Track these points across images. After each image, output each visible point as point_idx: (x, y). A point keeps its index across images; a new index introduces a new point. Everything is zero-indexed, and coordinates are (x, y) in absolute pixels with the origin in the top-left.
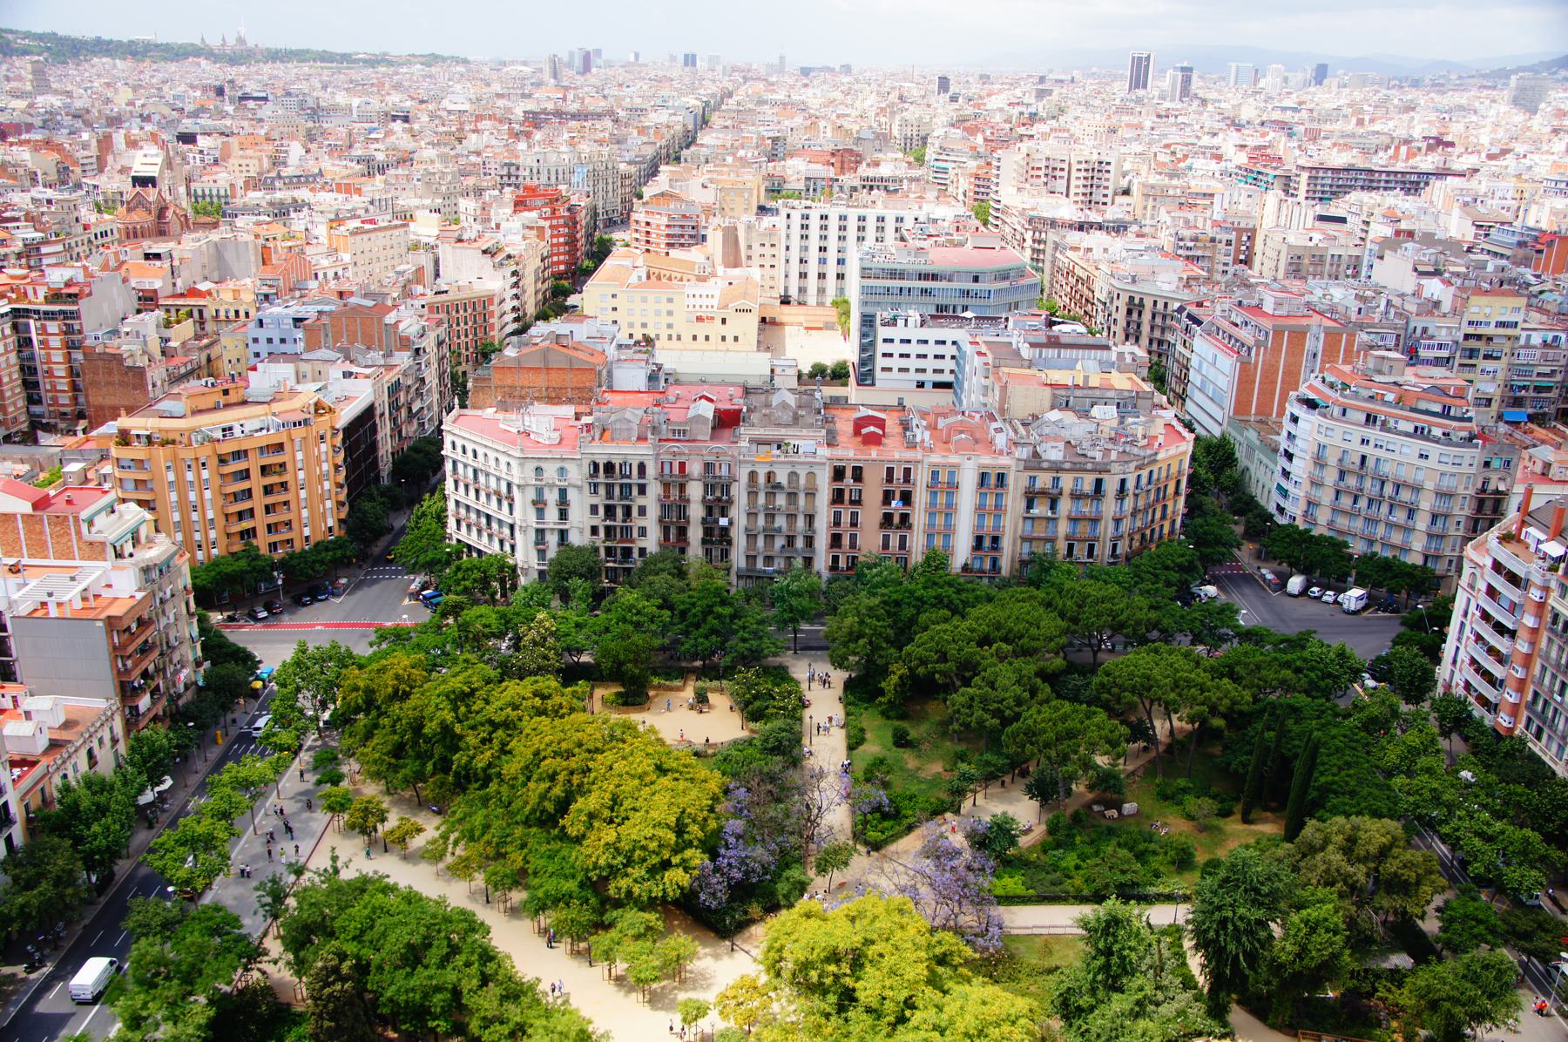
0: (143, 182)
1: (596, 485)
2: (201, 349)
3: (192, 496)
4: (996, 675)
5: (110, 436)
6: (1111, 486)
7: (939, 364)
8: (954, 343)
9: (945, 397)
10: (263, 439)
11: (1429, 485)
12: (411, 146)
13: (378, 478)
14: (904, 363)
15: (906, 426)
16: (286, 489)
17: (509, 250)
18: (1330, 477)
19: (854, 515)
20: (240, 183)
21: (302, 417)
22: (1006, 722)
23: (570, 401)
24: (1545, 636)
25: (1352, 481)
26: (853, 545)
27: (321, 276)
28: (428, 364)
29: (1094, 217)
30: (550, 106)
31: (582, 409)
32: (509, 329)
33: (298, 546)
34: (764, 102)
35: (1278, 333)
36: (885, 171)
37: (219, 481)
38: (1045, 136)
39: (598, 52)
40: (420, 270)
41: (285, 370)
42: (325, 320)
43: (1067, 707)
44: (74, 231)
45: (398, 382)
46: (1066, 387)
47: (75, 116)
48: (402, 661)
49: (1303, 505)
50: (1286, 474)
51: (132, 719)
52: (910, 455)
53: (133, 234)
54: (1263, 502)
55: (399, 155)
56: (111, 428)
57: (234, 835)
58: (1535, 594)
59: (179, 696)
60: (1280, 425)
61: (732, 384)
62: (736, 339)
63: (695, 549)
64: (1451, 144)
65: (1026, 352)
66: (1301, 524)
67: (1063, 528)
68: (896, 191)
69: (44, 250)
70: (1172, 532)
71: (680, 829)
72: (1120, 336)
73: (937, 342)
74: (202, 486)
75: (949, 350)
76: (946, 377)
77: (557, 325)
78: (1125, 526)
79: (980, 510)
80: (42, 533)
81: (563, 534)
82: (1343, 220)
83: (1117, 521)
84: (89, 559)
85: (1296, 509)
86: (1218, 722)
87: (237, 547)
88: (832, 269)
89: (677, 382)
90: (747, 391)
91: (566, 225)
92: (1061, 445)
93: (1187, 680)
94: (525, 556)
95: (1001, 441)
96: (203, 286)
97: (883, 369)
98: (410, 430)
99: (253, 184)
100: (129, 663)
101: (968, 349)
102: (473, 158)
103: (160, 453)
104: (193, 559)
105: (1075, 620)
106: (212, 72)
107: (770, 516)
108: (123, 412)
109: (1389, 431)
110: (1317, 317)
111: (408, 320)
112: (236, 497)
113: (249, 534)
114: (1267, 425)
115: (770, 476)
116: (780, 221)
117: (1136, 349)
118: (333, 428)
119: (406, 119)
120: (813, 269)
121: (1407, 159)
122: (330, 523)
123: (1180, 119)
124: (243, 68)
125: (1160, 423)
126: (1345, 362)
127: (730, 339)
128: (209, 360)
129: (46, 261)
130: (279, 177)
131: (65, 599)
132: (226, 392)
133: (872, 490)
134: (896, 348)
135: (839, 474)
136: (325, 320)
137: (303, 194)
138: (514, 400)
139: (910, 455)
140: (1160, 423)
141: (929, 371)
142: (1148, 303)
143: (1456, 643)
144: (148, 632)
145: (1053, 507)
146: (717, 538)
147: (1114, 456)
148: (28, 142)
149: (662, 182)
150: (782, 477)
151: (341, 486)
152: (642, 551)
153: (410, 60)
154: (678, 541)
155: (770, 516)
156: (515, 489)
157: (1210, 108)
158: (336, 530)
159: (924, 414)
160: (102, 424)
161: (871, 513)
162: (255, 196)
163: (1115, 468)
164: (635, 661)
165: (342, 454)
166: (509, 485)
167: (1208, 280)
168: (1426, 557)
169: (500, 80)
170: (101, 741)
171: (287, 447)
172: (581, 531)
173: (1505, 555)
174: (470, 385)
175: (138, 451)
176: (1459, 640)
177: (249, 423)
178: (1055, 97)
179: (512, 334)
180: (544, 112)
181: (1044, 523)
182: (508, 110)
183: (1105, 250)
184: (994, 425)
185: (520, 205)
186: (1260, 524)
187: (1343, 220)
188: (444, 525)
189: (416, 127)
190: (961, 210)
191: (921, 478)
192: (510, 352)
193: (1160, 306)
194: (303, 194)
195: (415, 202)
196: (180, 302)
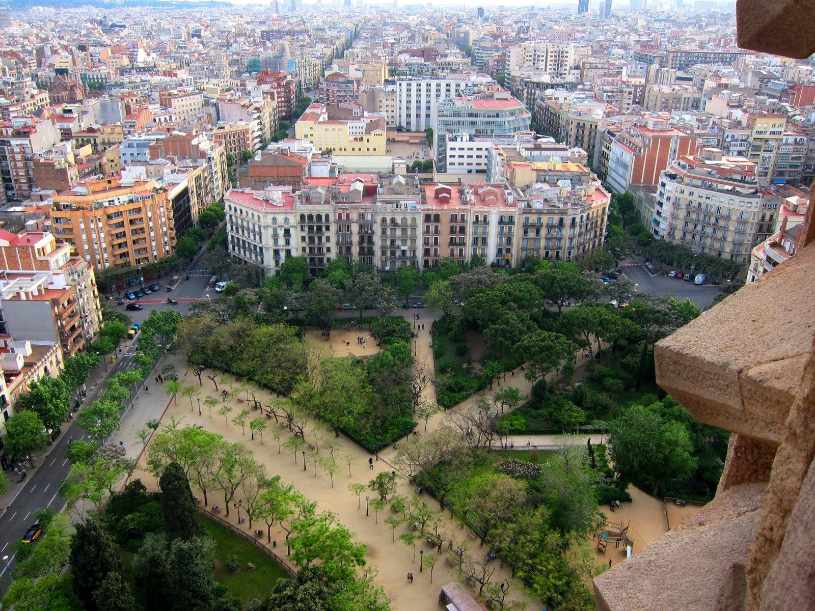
5: (50, 206)
6: (567, 221)
22: (513, 343)
59: (91, 339)
67: (543, 243)
74: (99, 231)
83: (571, 239)
86: (623, 342)
131: (29, 290)
135: (427, 218)
144: (73, 307)
145: (538, 233)
150: (399, 221)
170: (51, 363)
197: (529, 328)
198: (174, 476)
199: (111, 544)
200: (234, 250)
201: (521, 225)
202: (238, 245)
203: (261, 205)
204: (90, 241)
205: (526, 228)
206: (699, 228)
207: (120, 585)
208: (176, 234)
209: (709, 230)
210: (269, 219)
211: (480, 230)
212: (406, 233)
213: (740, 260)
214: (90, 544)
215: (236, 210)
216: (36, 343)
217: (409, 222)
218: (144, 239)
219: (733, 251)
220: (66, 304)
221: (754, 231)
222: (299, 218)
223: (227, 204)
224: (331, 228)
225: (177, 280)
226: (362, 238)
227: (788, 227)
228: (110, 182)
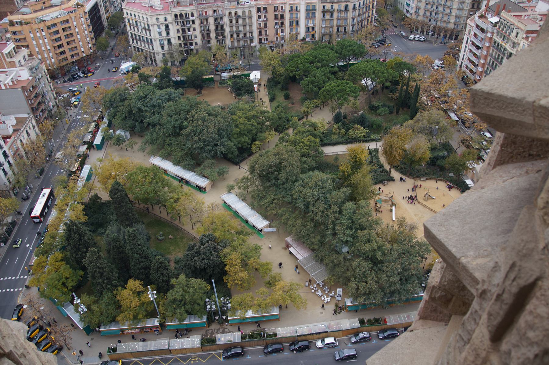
1: (177, 22)
3: (41, 42)
4: (316, 73)
5: (7, 23)
6: (351, 7)
16: (73, 36)
21: (72, 9)
22: (320, 89)
24: (492, 48)
26: (266, 34)
37: (49, 35)
43: (340, 82)
49: (415, 9)
56: (6, 20)
58: (489, 35)
59: (51, 110)
63: (214, 41)
67: (335, 22)
71: (220, 134)
74: (43, 38)
78: (356, 20)
83: (353, 19)
86: (388, 84)
93: (378, 70)
98: (112, 10)
100: (33, 101)
103: (26, 28)
108: (9, 14)
113: (63, 53)
115: (236, 13)
118: (85, 12)
122: (90, 45)
131: (6, 82)
135: (259, 10)
143: (465, 45)
144: (36, 90)
145: (332, 15)
150: (240, 13)
154: (208, 38)
155: (237, 27)
156: (150, 26)
158: (92, 48)
160: (2, 19)
165: (89, 21)
166: (148, 25)
168: (455, 25)
170: (29, 127)
171: (70, 21)
172: (175, 38)
173: (480, 22)
176: (465, 52)
181: (329, 21)
197: (328, 79)
198: (117, 189)
199: (87, 232)
200: (133, 42)
201: (321, 11)
202: (136, 38)
203: (148, 11)
204: (38, 45)
205: (324, 14)
206: (435, 7)
207: (97, 255)
208: (94, 35)
209: (441, 9)
210: (154, 21)
211: (294, 16)
212: (246, 22)
213: (459, 28)
214: (75, 233)
215: (131, 15)
216: (17, 116)
217: (247, 14)
218: (74, 40)
219: (455, 22)
220: (31, 89)
221: (469, 8)
222: (174, 17)
223: (125, 12)
224: (196, 22)
225: (99, 66)
226: (217, 27)
227: (490, 5)
228: (44, 3)
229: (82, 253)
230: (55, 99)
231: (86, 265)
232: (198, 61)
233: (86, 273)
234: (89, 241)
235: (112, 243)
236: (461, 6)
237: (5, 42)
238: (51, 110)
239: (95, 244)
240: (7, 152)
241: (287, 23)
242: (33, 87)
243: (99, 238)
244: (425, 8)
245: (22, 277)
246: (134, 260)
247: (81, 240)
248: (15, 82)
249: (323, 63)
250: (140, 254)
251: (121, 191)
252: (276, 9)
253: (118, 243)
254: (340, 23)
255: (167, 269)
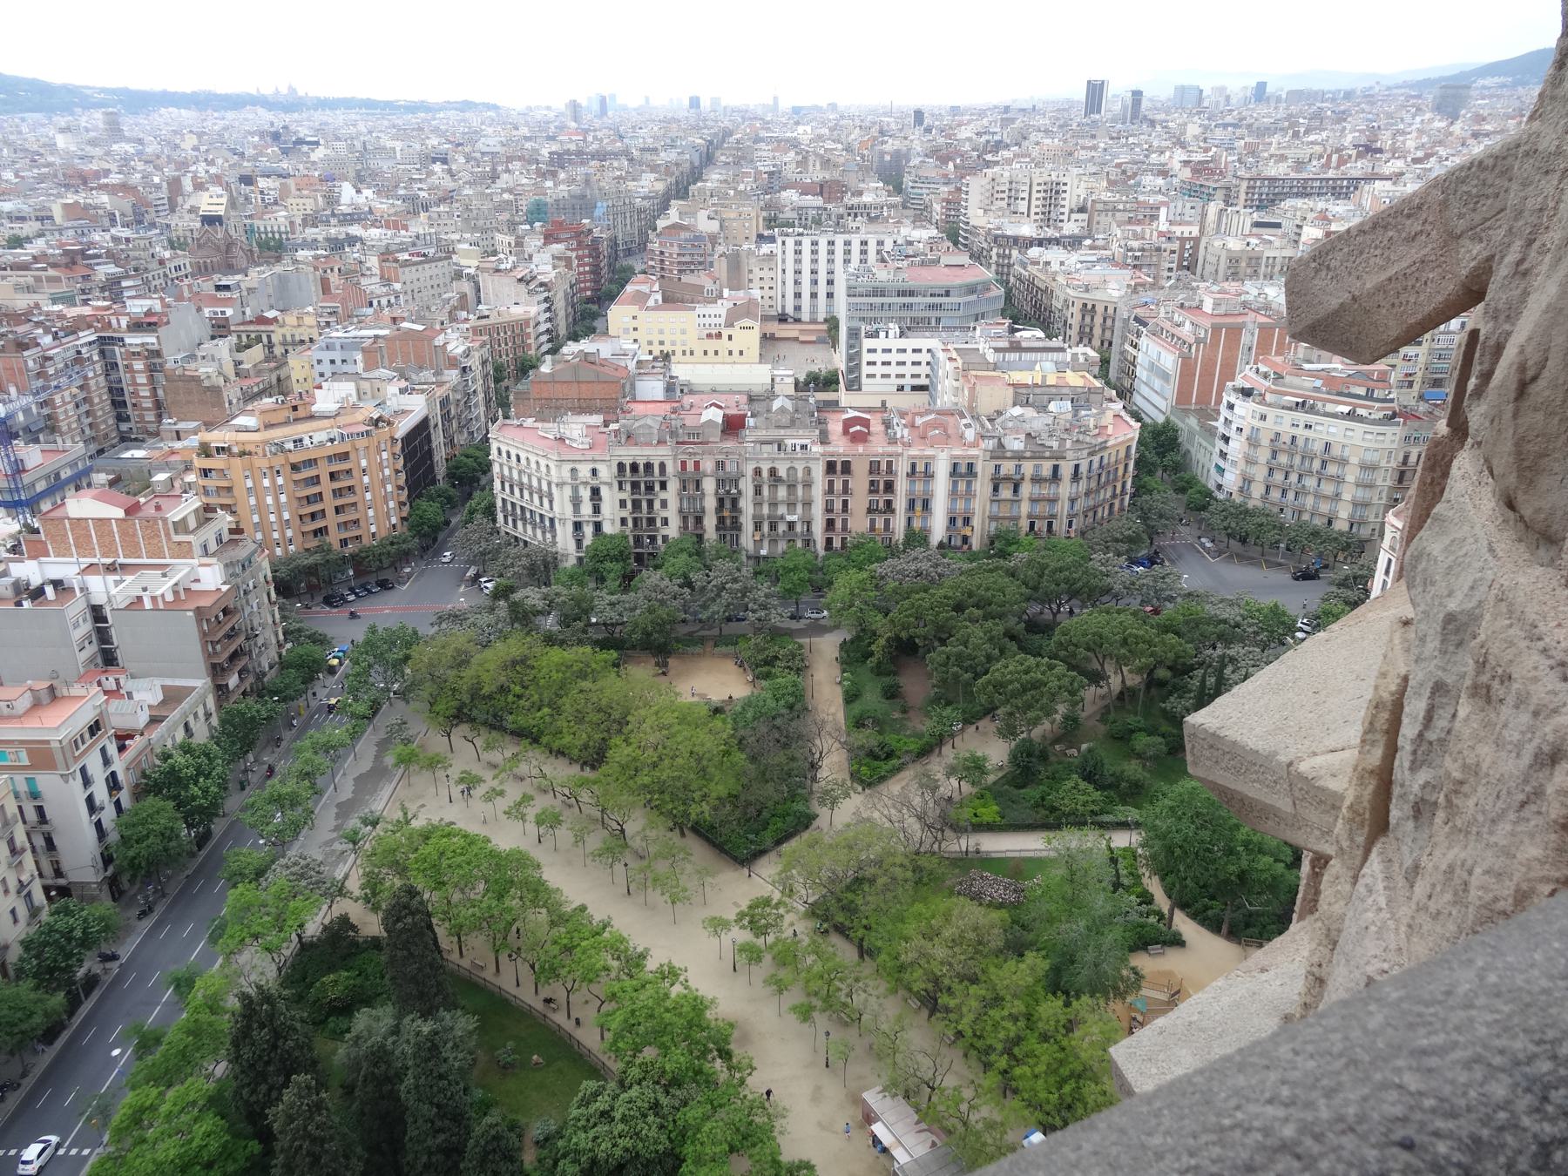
0: (210, 220)
2: (271, 370)
3: (269, 500)
6: (1066, 470)
7: (916, 370)
8: (929, 351)
9: (921, 398)
10: (331, 449)
11: (1354, 460)
12: (451, 185)
13: (434, 481)
14: (886, 370)
15: (887, 425)
17: (541, 278)
18: (1263, 455)
19: (846, 483)
20: (298, 221)
22: (977, 676)
23: (598, 411)
25: (1283, 459)
26: (845, 528)
27: (375, 303)
28: (474, 380)
29: (1050, 233)
30: (573, 147)
31: (611, 417)
32: (545, 348)
33: (366, 541)
34: (761, 140)
35: (1216, 329)
36: (867, 198)
38: (1009, 162)
39: (613, 97)
40: (463, 297)
41: (347, 388)
42: (381, 343)
43: (1031, 661)
44: (150, 267)
45: (448, 397)
46: (1026, 386)
47: (147, 162)
48: (460, 637)
50: (1223, 455)
51: (221, 690)
52: (891, 449)
53: (202, 270)
54: (1203, 481)
55: (440, 193)
57: (319, 793)
59: (264, 674)
60: (1218, 413)
61: (740, 393)
62: (741, 353)
64: (1380, 151)
65: (991, 357)
66: (1237, 498)
67: (1025, 508)
68: (877, 217)
69: (124, 284)
70: (1122, 509)
72: (1075, 338)
73: (914, 351)
75: (924, 357)
76: (923, 381)
77: (586, 345)
79: (953, 494)
80: (135, 535)
81: (598, 526)
82: (1278, 226)
83: (1073, 501)
84: (178, 557)
85: (1231, 480)
86: (1162, 673)
87: (313, 543)
88: (822, 289)
89: (691, 392)
90: (751, 399)
91: (590, 256)
92: (1023, 437)
93: (1136, 637)
94: (565, 541)
95: (970, 435)
96: (270, 314)
97: (868, 376)
98: (462, 439)
99: (312, 220)
100: (218, 647)
101: (941, 356)
102: (506, 196)
104: (271, 556)
105: (1035, 589)
106: (266, 118)
107: (774, 505)
109: (1317, 413)
110: (1252, 315)
111: (456, 344)
112: (309, 500)
114: (1207, 413)
115: (773, 472)
116: (776, 248)
117: (1089, 351)
118: (392, 438)
119: (444, 161)
120: (806, 290)
121: (1338, 167)
122: (394, 520)
123: (1131, 140)
124: (296, 115)
125: (1110, 414)
126: (1278, 353)
127: (736, 353)
128: (279, 380)
129: (126, 294)
130: (333, 215)
131: (159, 593)
132: (295, 408)
133: (860, 481)
134: (879, 357)
135: (831, 467)
136: (381, 343)
137: (355, 230)
138: (551, 409)
139: (891, 449)
140: (1110, 414)
141: (908, 376)
142: (1100, 309)
145: (1016, 491)
146: (729, 525)
147: (1068, 444)
148: (107, 185)
149: (673, 215)
150: (782, 473)
151: (400, 488)
152: (665, 538)
153: (447, 106)
155: (774, 505)
157: (1158, 128)
158: (399, 527)
159: (902, 414)
161: (860, 499)
162: (311, 233)
163: (1070, 455)
164: (659, 632)
165: (401, 461)
166: (549, 484)
167: (1153, 286)
169: (527, 124)
170: (196, 715)
171: (352, 456)
172: (613, 522)
174: (511, 398)
175: (216, 462)
177: (317, 436)
178: (1018, 124)
179: (547, 353)
180: (568, 152)
182: (536, 151)
183: (1062, 263)
184: (964, 421)
185: (549, 238)
186: (1201, 502)
187: (1278, 226)
188: (494, 521)
189: (454, 167)
190: (934, 232)
191: (902, 468)
192: (545, 368)
193: (1111, 311)
194: (355, 230)
195: (456, 237)
196: (252, 328)
197: (1002, 651)
199: (298, 1025)
202: (514, 514)
204: (260, 508)
206: (1294, 478)
208: (409, 496)
210: (566, 475)
212: (795, 494)
213: (1365, 532)
214: (262, 1026)
216: (169, 682)
217: (800, 474)
218: (354, 504)
221: (1389, 483)
222: (615, 469)
223: (494, 446)
224: (669, 486)
226: (721, 501)
229: (270, 1089)
230: (280, 646)
231: (276, 1126)
232: (667, 582)
233: (268, 1152)
234: (297, 1053)
235: (365, 1064)
236: (1367, 477)
237: (177, 492)
238: (264, 674)
239: (312, 1065)
240: (121, 777)
241: (900, 504)
242: (226, 611)
243: (331, 1045)
244: (1266, 480)
245: (74, 1152)
246: (420, 1121)
247: (275, 1047)
248: (183, 594)
249: (989, 609)
250: (438, 1106)
251: (418, 911)
252: (874, 468)
253: (384, 1067)
254: (1039, 509)
255: (512, 1160)
